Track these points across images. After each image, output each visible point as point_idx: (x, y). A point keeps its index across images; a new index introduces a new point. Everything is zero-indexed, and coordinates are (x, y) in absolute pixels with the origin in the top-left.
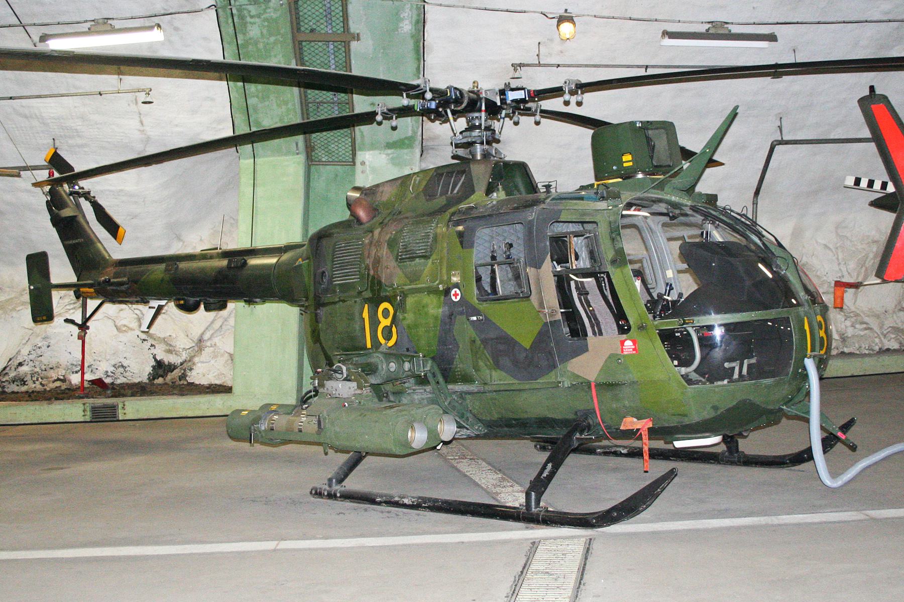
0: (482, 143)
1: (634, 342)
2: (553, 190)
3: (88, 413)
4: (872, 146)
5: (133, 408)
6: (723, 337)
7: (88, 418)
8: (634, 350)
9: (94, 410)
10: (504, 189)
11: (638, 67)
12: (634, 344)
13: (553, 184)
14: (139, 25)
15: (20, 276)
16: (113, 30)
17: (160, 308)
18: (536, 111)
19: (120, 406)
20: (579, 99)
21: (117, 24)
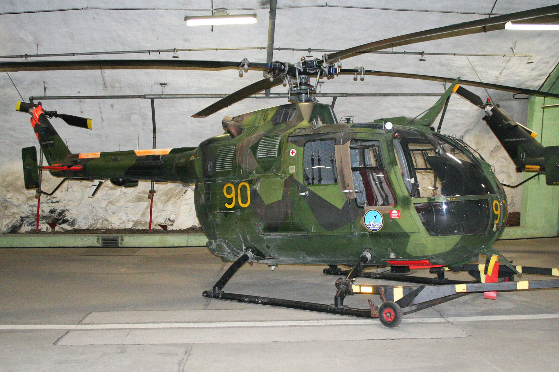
0: (306, 94)
1: (398, 211)
2: (351, 122)
3: (101, 241)
4: (546, 91)
5: (129, 241)
6: (446, 209)
7: (100, 245)
8: (398, 216)
9: (104, 240)
10: (321, 120)
11: (21, 56)
12: (398, 213)
13: (352, 118)
14: (244, 14)
15: (17, 167)
16: (228, 16)
17: (101, 184)
18: (361, 71)
19: (120, 239)
20: (340, 64)
21: (231, 12)
